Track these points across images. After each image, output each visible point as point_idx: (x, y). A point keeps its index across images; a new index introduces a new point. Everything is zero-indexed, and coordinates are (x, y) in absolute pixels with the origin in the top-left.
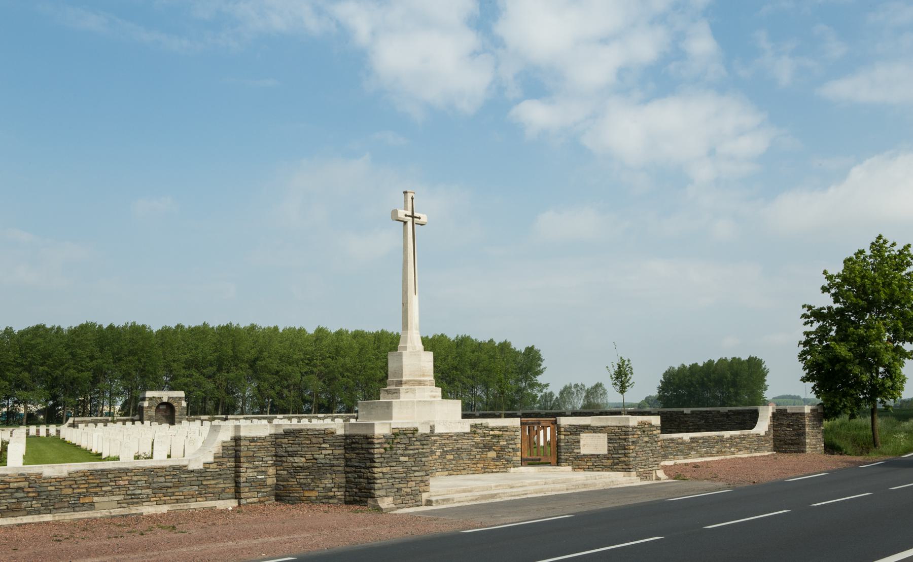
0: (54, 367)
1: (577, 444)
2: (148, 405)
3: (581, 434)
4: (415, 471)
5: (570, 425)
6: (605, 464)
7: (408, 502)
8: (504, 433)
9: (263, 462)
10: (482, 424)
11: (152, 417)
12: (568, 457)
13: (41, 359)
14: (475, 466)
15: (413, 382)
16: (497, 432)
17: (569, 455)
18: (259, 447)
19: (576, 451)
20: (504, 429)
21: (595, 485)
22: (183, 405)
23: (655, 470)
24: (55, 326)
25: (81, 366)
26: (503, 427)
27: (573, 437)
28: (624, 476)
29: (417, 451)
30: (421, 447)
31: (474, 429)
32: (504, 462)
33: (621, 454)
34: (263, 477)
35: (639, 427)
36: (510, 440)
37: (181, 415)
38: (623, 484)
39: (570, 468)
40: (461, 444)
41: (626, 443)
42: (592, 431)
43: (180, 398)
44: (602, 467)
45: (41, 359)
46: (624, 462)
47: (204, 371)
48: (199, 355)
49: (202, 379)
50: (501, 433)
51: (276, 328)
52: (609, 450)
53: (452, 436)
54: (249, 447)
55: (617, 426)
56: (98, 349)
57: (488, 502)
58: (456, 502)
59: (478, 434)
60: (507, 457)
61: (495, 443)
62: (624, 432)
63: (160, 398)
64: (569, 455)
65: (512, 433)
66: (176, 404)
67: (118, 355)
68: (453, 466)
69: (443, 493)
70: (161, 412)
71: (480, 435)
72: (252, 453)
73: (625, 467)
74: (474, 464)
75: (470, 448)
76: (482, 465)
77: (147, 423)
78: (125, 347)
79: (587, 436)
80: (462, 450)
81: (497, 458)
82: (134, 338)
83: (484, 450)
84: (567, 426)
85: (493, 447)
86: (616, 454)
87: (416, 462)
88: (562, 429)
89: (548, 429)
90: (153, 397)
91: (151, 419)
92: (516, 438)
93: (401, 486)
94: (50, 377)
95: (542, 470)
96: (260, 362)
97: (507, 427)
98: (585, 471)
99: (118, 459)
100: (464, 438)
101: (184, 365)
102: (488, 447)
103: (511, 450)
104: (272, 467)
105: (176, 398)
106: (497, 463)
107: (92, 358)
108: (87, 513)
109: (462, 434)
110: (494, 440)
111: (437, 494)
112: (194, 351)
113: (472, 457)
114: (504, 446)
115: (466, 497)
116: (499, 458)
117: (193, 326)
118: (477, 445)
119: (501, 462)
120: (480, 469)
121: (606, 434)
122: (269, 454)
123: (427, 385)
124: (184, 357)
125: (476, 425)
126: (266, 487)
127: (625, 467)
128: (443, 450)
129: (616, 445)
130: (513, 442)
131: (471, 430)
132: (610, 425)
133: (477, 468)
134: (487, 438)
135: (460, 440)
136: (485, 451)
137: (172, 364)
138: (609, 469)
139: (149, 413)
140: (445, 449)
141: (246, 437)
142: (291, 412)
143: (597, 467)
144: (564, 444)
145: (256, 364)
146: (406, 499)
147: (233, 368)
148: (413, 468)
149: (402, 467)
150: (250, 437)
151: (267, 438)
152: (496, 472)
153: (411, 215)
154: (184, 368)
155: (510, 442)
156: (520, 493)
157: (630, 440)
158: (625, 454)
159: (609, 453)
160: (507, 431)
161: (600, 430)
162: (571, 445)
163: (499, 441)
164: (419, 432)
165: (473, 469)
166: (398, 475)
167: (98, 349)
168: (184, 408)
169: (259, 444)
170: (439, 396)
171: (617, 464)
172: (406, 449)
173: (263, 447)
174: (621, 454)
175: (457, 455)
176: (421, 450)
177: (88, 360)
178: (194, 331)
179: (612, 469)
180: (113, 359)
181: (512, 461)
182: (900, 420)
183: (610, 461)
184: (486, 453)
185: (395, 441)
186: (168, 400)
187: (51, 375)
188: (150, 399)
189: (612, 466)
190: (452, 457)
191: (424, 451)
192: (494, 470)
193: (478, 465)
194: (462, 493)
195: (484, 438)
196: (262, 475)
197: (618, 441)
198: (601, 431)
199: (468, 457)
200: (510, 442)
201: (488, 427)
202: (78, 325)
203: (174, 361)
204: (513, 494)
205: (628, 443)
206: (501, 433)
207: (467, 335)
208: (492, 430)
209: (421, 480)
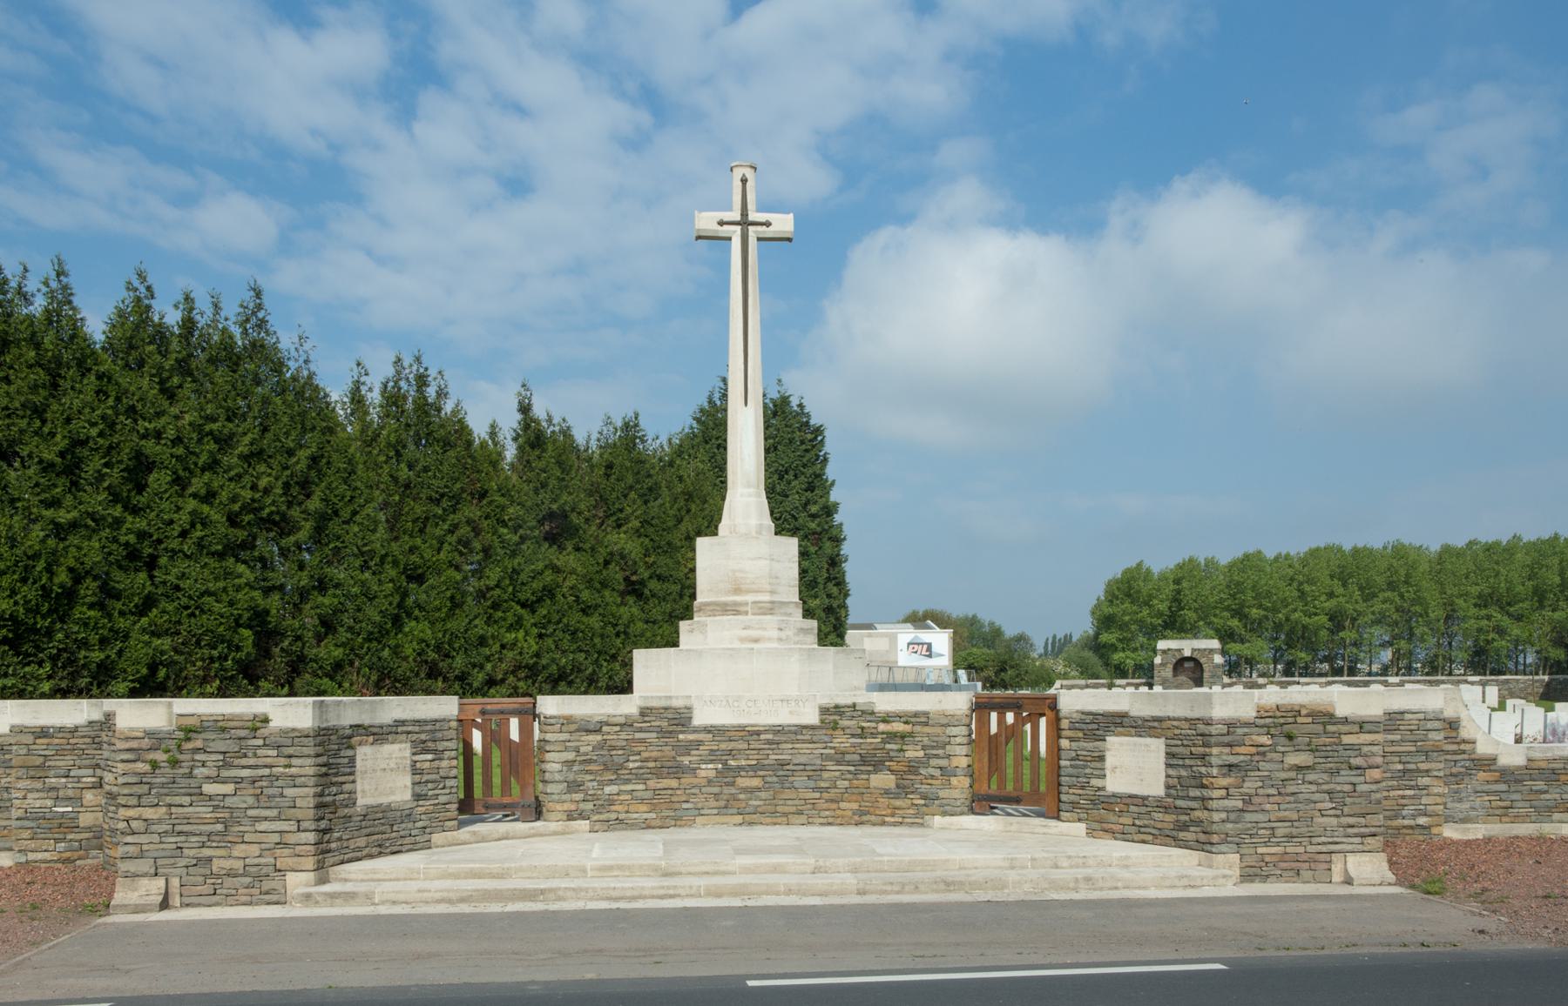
1: (1098, 765)
3: (1107, 738)
4: (257, 819)
5: (1083, 713)
6: (1159, 825)
7: (234, 892)
8: (918, 728)
9: (70, 780)
10: (854, 705)
12: (1076, 798)
14: (834, 806)
15: (711, 608)
16: (898, 727)
17: (1080, 792)
18: (57, 748)
19: (1095, 782)
20: (918, 720)
21: (1001, 885)
23: (1344, 852)
24: (1280, 554)
26: (916, 715)
27: (1090, 745)
28: (1199, 865)
29: (266, 771)
30: (283, 761)
31: (832, 718)
32: (916, 802)
33: (1194, 799)
34: (70, 809)
35: (1262, 722)
36: (933, 748)
37: (1212, 677)
38: (1145, 888)
39: (1082, 827)
40: (790, 751)
41: (1203, 770)
42: (1133, 730)
43: (1211, 651)
44: (1153, 831)
46: (1199, 822)
47: (1512, 609)
48: (1502, 585)
49: (1506, 622)
50: (908, 728)
52: (1168, 787)
53: (758, 733)
54: (32, 747)
55: (1186, 719)
57: (478, 910)
58: (383, 903)
59: (843, 729)
60: (924, 788)
61: (892, 754)
62: (1201, 735)
63: (1179, 650)
64: (1080, 792)
65: (938, 730)
68: (761, 803)
69: (392, 877)
71: (848, 731)
72: (42, 759)
73: (1202, 837)
74: (832, 801)
75: (819, 762)
76: (855, 806)
77: (1158, 689)
79: (1121, 744)
80: (794, 768)
81: (897, 791)
83: (862, 768)
84: (1075, 715)
85: (887, 763)
86: (1183, 798)
87: (263, 798)
88: (1065, 724)
89: (1043, 721)
90: (1169, 650)
91: (1165, 684)
92: (949, 743)
93: (207, 852)
95: (1014, 828)
97: (926, 714)
98: (1116, 839)
100: (799, 737)
101: (1476, 600)
102: (873, 762)
103: (937, 773)
104: (93, 790)
105: (1205, 650)
106: (898, 803)
107: (1331, 595)
108: (1018, 823)
109: (793, 728)
110: (888, 746)
111: (371, 876)
112: (1492, 580)
113: (823, 784)
114: (918, 760)
115: (419, 891)
116: (902, 790)
117: (1490, 542)
118: (840, 757)
119: (909, 802)
120: (850, 813)
121: (1163, 740)
122: (87, 762)
123: (746, 613)
124: (1475, 590)
125: (837, 707)
126: (76, 830)
127: (1202, 837)
128: (725, 763)
129: (1184, 773)
130: (940, 752)
131: (822, 721)
132: (1171, 714)
133: (838, 812)
134: (869, 740)
135: (785, 742)
136: (862, 772)
137: (1457, 601)
138: (1169, 840)
139: (1163, 673)
140: (732, 763)
141: (26, 727)
142: (1346, 672)
143: (1142, 830)
144: (1068, 763)
146: (225, 885)
148: (251, 813)
149: (211, 809)
150: (35, 727)
151: (80, 729)
152: (895, 824)
153: (738, 218)
154: (1475, 605)
155: (934, 752)
156: (646, 893)
157: (1214, 760)
158: (1203, 799)
159: (1168, 795)
160: (926, 724)
161: (1150, 728)
162: (1085, 767)
163: (905, 747)
164: (271, 724)
165: (827, 813)
166: (195, 827)
168: (1218, 666)
169: (57, 741)
171: (1184, 827)
172: (227, 765)
173: (69, 747)
174: (1194, 799)
175: (775, 779)
176: (281, 769)
177: (1323, 598)
179: (1175, 839)
181: (938, 798)
183: (1170, 818)
184: (865, 777)
185: (189, 745)
188: (1164, 652)
189: (1174, 833)
190: (756, 782)
191: (293, 770)
192: (887, 819)
193: (842, 805)
194: (466, 878)
195: (861, 741)
196: (67, 806)
197: (1188, 762)
198: (1152, 731)
199: (812, 784)
200: (934, 752)
201: (873, 713)
202: (1306, 549)
204: (614, 894)
205: (1209, 769)
206: (908, 728)
208: (884, 721)
209: (278, 840)
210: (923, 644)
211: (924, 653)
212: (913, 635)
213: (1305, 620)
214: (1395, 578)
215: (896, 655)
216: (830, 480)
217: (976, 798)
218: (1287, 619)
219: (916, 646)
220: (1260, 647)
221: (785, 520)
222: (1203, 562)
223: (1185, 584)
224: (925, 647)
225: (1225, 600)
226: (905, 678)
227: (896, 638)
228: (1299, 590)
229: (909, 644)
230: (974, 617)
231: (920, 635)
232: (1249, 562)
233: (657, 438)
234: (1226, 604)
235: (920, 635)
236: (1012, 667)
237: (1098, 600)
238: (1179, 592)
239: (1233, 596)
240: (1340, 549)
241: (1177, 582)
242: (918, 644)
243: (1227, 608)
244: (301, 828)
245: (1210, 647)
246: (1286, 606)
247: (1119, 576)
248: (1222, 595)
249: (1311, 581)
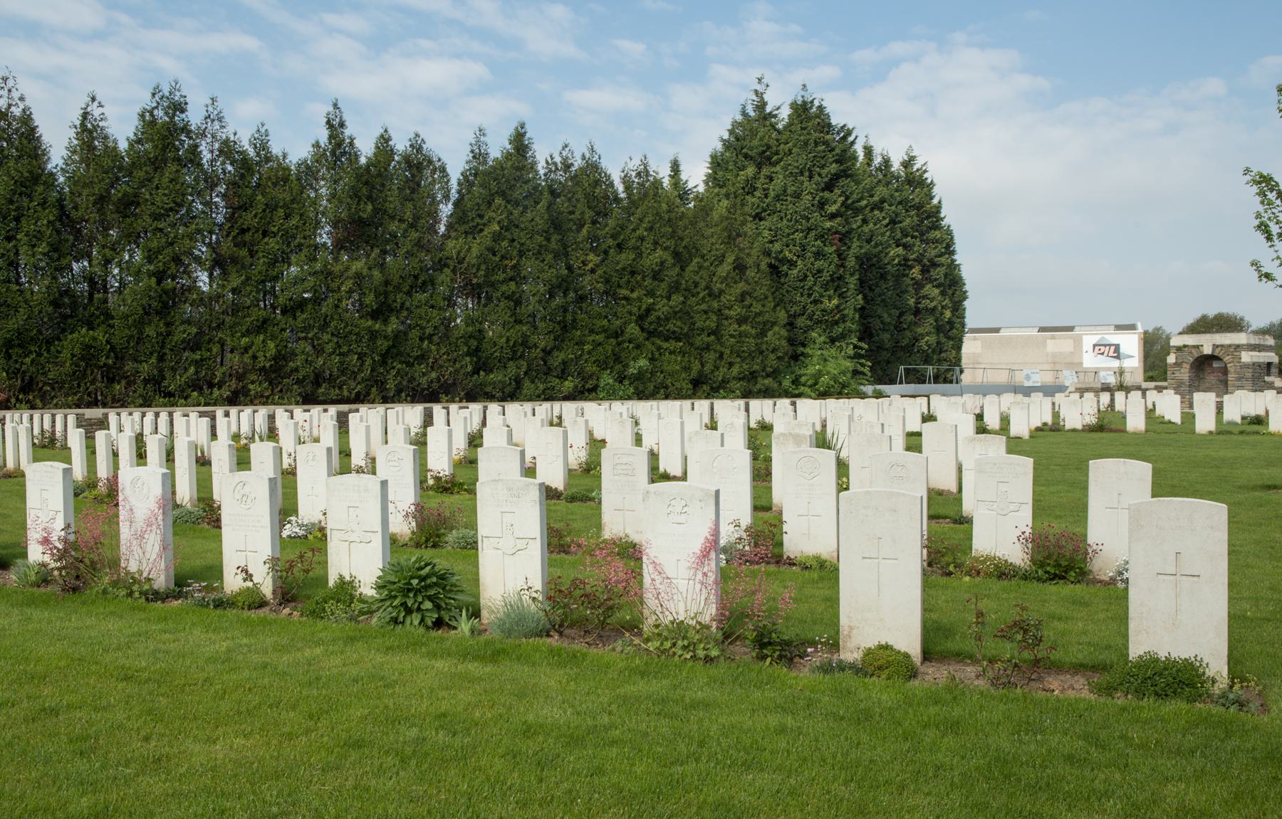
2: (1174, 361)
11: (1184, 383)
22: (1243, 360)
37: (1239, 379)
63: (1197, 347)
66: (1228, 358)
70: (1215, 374)
90: (1185, 346)
105: (1230, 346)
170: (681, 406)
186: (1213, 350)
188: (1179, 349)
207: (966, 282)
210: (1110, 345)
211: (1111, 354)
215: (1081, 357)
216: (280, 154)
219: (1103, 348)
221: (797, 221)
224: (1113, 348)
226: (985, 380)
227: (1081, 339)
229: (1095, 346)
231: (1107, 337)
233: (566, 146)
235: (1107, 337)
242: (1105, 345)
244: (347, 543)
245: (1237, 342)
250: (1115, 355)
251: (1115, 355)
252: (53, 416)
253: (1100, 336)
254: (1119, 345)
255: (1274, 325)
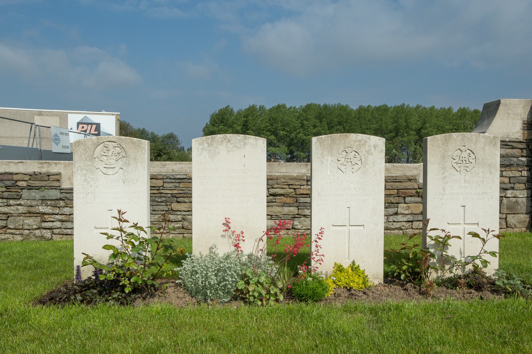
0: (290, 132)
13: (282, 126)
24: (421, 106)
25: (308, 132)
45: (282, 126)
51: (450, 109)
56: (319, 121)
67: (331, 124)
78: (335, 119)
82: (341, 114)
94: (289, 138)
96: (424, 131)
99: (60, 187)
107: (315, 127)
145: (421, 132)
147: (405, 134)
167: (319, 121)
177: (312, 128)
178: (378, 109)
180: (328, 126)
182: (527, 166)
187: (289, 137)
203: (367, 129)
210: (92, 124)
211: (93, 132)
212: (82, 116)
213: (305, 137)
214: (342, 120)
217: (129, 295)
218: (296, 137)
219: (86, 126)
220: (283, 149)
222: (258, 107)
223: (250, 118)
225: (268, 126)
227: (67, 117)
228: (301, 123)
229: (78, 124)
230: (144, 129)
231: (89, 116)
232: (279, 108)
234: (268, 128)
235: (89, 116)
236: (164, 154)
237: (206, 124)
238: (246, 122)
239: (272, 125)
240: (319, 105)
241: (246, 116)
242: (88, 124)
243: (269, 130)
246: (296, 131)
247: (217, 112)
248: (267, 124)
249: (307, 119)
250: (96, 133)
251: (96, 133)
252: (32, 146)
253: (84, 115)
254: (99, 124)
255: (231, 112)
